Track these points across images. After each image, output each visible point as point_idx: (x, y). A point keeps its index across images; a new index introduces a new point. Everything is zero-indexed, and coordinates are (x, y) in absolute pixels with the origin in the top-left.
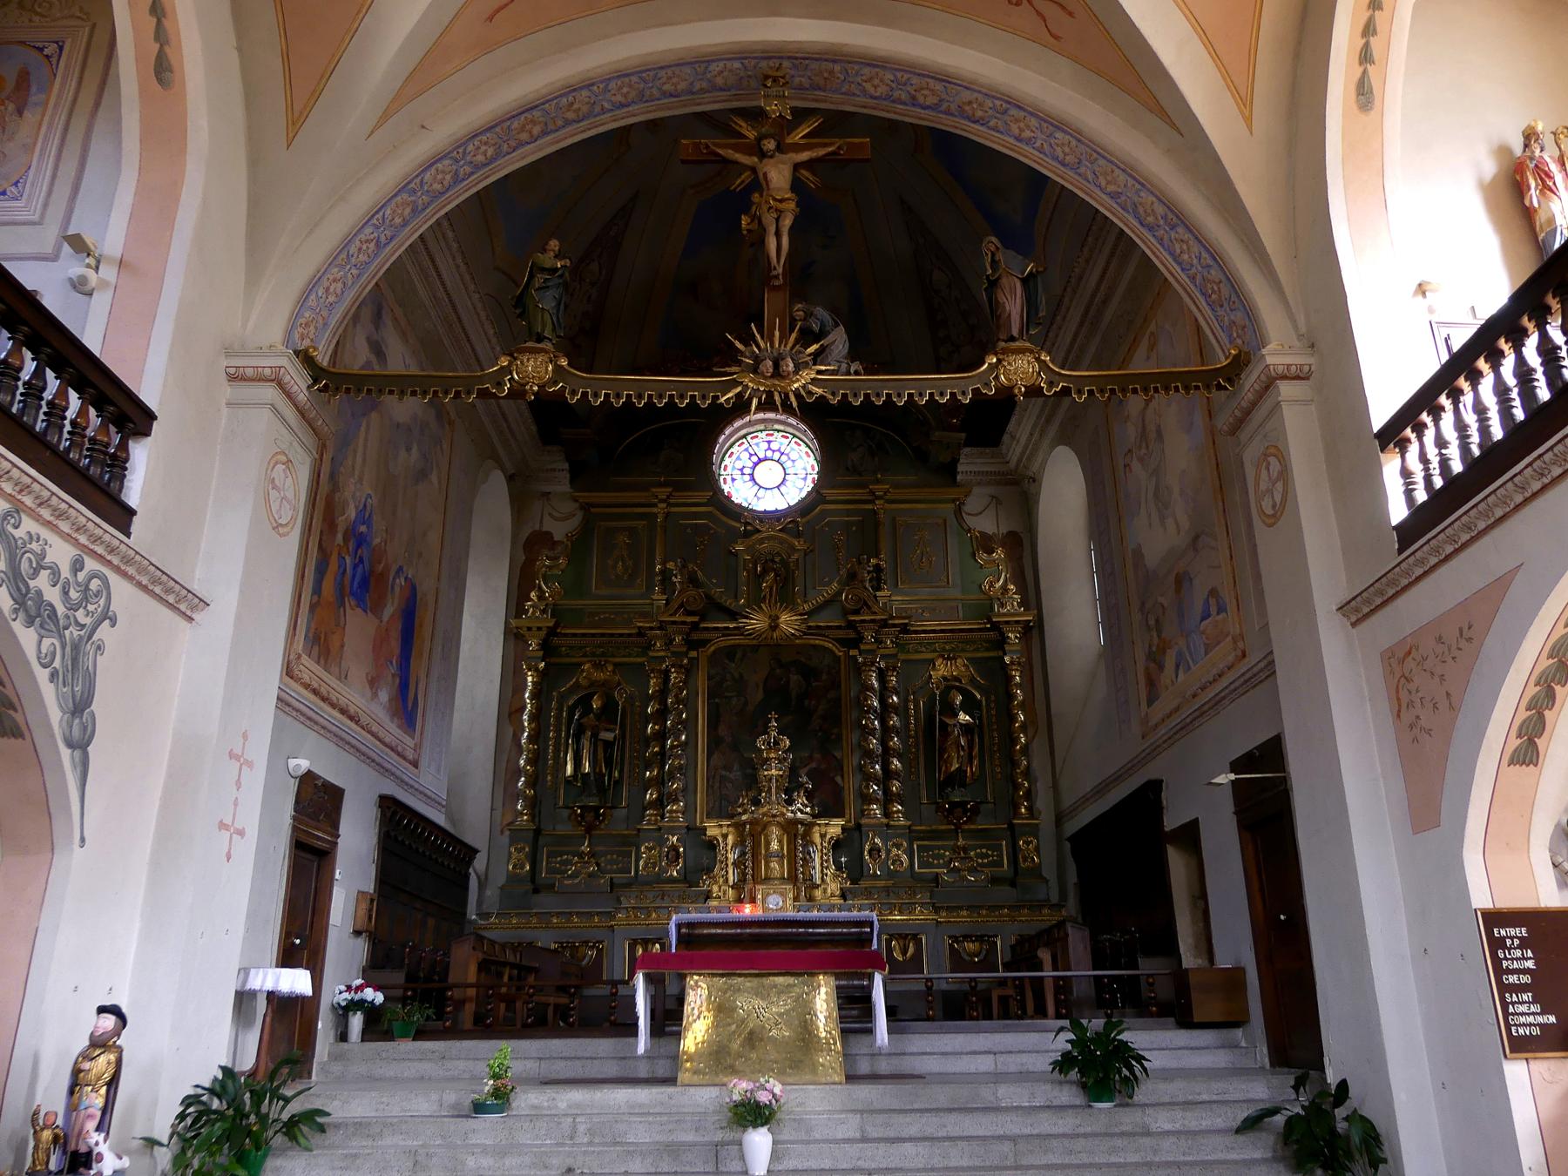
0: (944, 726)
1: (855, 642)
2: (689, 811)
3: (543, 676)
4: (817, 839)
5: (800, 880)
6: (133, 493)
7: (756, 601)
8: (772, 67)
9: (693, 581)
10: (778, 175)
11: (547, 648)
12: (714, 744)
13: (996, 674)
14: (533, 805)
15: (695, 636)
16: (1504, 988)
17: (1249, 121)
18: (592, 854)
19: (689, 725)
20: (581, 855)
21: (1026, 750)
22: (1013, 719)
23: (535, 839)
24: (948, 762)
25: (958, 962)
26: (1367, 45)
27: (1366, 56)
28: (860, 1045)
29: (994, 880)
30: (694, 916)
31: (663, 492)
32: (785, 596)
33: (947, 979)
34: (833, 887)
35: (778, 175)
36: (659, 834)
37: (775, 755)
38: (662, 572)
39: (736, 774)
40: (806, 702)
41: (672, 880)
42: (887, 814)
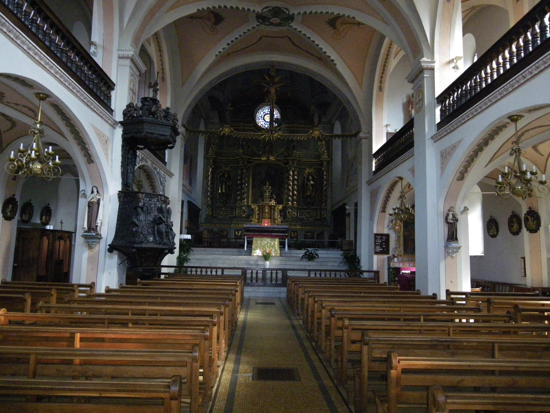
0: (307, 184)
1: (288, 163)
2: (248, 202)
5: (272, 218)
6: (166, 161)
8: (272, 64)
10: (273, 91)
11: (214, 162)
13: (320, 172)
14: (212, 199)
16: (375, 245)
17: (361, 88)
20: (223, 211)
22: (323, 183)
25: (306, 237)
26: (381, 80)
27: (381, 82)
28: (283, 251)
29: (316, 220)
30: (248, 226)
31: (242, 124)
33: (301, 239)
34: (279, 220)
35: (273, 91)
36: (241, 207)
37: (268, 190)
40: (275, 178)
41: (244, 217)
42: (292, 204)
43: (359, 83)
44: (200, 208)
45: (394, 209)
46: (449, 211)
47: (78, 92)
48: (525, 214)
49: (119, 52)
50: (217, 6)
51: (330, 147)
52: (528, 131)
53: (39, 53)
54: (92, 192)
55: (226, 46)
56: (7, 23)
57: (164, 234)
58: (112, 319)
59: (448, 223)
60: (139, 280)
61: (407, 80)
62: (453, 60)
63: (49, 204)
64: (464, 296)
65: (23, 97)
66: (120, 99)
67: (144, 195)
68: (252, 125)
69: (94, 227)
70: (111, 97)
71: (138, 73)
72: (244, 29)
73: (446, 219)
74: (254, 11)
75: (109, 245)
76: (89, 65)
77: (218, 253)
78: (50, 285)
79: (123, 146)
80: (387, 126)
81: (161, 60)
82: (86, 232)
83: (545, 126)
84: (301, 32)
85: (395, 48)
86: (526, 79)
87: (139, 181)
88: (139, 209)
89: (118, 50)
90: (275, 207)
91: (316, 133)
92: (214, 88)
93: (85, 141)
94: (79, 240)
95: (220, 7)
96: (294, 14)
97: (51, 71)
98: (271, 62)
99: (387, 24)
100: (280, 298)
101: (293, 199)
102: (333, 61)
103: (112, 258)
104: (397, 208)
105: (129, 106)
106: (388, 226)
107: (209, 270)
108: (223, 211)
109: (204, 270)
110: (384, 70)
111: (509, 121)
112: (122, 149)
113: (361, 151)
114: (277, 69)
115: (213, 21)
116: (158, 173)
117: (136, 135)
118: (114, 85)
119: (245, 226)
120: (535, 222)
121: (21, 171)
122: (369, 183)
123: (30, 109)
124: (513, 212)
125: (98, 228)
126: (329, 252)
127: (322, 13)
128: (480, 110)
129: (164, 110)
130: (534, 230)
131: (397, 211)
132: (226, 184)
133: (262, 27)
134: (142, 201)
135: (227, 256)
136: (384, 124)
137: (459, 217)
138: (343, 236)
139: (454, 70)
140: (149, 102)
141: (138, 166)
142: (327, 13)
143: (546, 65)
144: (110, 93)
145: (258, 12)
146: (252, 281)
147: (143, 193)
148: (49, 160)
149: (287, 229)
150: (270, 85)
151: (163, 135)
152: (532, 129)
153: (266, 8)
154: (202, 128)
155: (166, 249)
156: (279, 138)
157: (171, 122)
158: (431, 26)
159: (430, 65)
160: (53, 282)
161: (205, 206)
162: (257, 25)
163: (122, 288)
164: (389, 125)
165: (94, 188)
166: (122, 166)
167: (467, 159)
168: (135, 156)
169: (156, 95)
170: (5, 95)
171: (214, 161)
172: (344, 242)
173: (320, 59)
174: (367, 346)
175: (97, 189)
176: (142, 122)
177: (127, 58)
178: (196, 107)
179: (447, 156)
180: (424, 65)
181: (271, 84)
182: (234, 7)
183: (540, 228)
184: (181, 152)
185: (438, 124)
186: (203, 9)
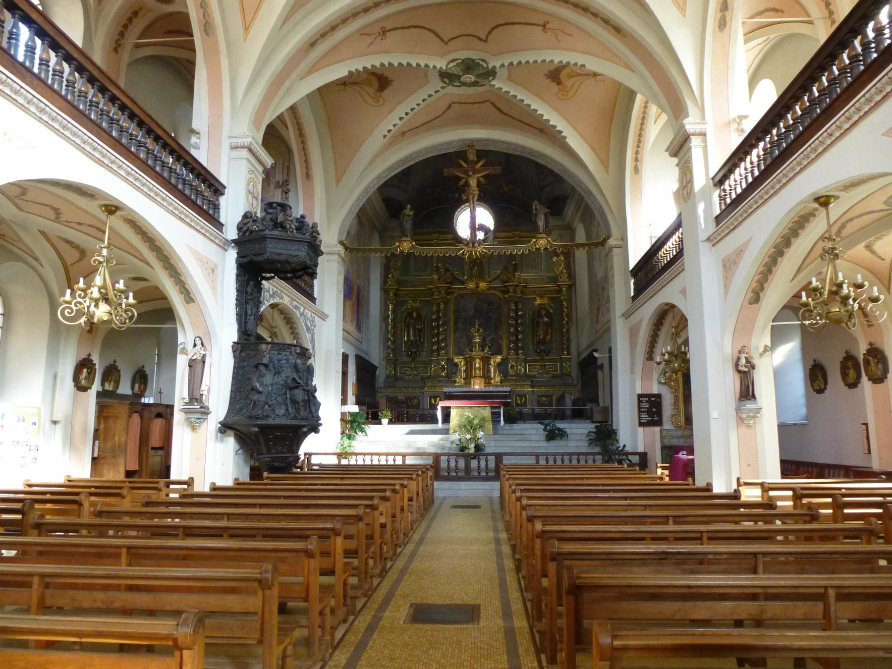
0: (538, 322)
3: (395, 305)
4: (492, 363)
5: (487, 378)
6: (315, 296)
7: (471, 277)
8: (471, 144)
9: (447, 270)
10: (473, 183)
12: (456, 329)
15: (449, 290)
16: (640, 412)
17: (607, 172)
18: (415, 368)
23: (393, 362)
25: (540, 404)
27: (636, 160)
29: (554, 377)
30: (451, 390)
31: (436, 236)
32: (481, 276)
34: (498, 379)
35: (473, 183)
38: (437, 266)
39: (464, 340)
41: (443, 377)
43: (602, 161)
46: (740, 352)
47: (164, 199)
50: (378, 65)
51: (572, 265)
52: (851, 220)
54: (195, 345)
56: (47, 108)
57: (301, 404)
58: (189, 528)
59: (739, 372)
60: (265, 474)
61: (667, 153)
63: (143, 367)
65: (85, 211)
67: (269, 346)
70: (219, 205)
71: (261, 169)
73: (737, 365)
74: (434, 67)
75: (220, 423)
79: (238, 276)
82: (187, 404)
86: (833, 138)
88: (262, 368)
89: (230, 138)
91: (542, 242)
94: (178, 417)
96: (494, 67)
98: (469, 140)
99: (633, 71)
102: (561, 132)
105: (246, 216)
108: (411, 368)
110: (639, 141)
111: (816, 205)
113: (612, 267)
114: (478, 151)
115: (377, 87)
116: (302, 314)
117: (255, 259)
118: (225, 187)
119: (445, 390)
120: (880, 366)
124: (847, 352)
125: (204, 397)
127: (536, 62)
128: (772, 192)
129: (297, 219)
130: (878, 379)
131: (666, 357)
132: (414, 329)
133: (450, 89)
134: (268, 356)
137: (756, 361)
138: (595, 400)
140: (275, 208)
141: (267, 304)
142: (544, 61)
143: (861, 114)
144: (218, 200)
145: (441, 68)
152: (858, 217)
153: (452, 61)
155: (304, 426)
157: (307, 236)
161: (384, 363)
162: (442, 88)
163: (238, 484)
167: (761, 269)
168: (259, 288)
170: (61, 211)
171: (395, 295)
173: (542, 131)
174: (555, 563)
175: (201, 339)
176: (264, 238)
183: (889, 375)
184: (338, 281)
185: (717, 218)
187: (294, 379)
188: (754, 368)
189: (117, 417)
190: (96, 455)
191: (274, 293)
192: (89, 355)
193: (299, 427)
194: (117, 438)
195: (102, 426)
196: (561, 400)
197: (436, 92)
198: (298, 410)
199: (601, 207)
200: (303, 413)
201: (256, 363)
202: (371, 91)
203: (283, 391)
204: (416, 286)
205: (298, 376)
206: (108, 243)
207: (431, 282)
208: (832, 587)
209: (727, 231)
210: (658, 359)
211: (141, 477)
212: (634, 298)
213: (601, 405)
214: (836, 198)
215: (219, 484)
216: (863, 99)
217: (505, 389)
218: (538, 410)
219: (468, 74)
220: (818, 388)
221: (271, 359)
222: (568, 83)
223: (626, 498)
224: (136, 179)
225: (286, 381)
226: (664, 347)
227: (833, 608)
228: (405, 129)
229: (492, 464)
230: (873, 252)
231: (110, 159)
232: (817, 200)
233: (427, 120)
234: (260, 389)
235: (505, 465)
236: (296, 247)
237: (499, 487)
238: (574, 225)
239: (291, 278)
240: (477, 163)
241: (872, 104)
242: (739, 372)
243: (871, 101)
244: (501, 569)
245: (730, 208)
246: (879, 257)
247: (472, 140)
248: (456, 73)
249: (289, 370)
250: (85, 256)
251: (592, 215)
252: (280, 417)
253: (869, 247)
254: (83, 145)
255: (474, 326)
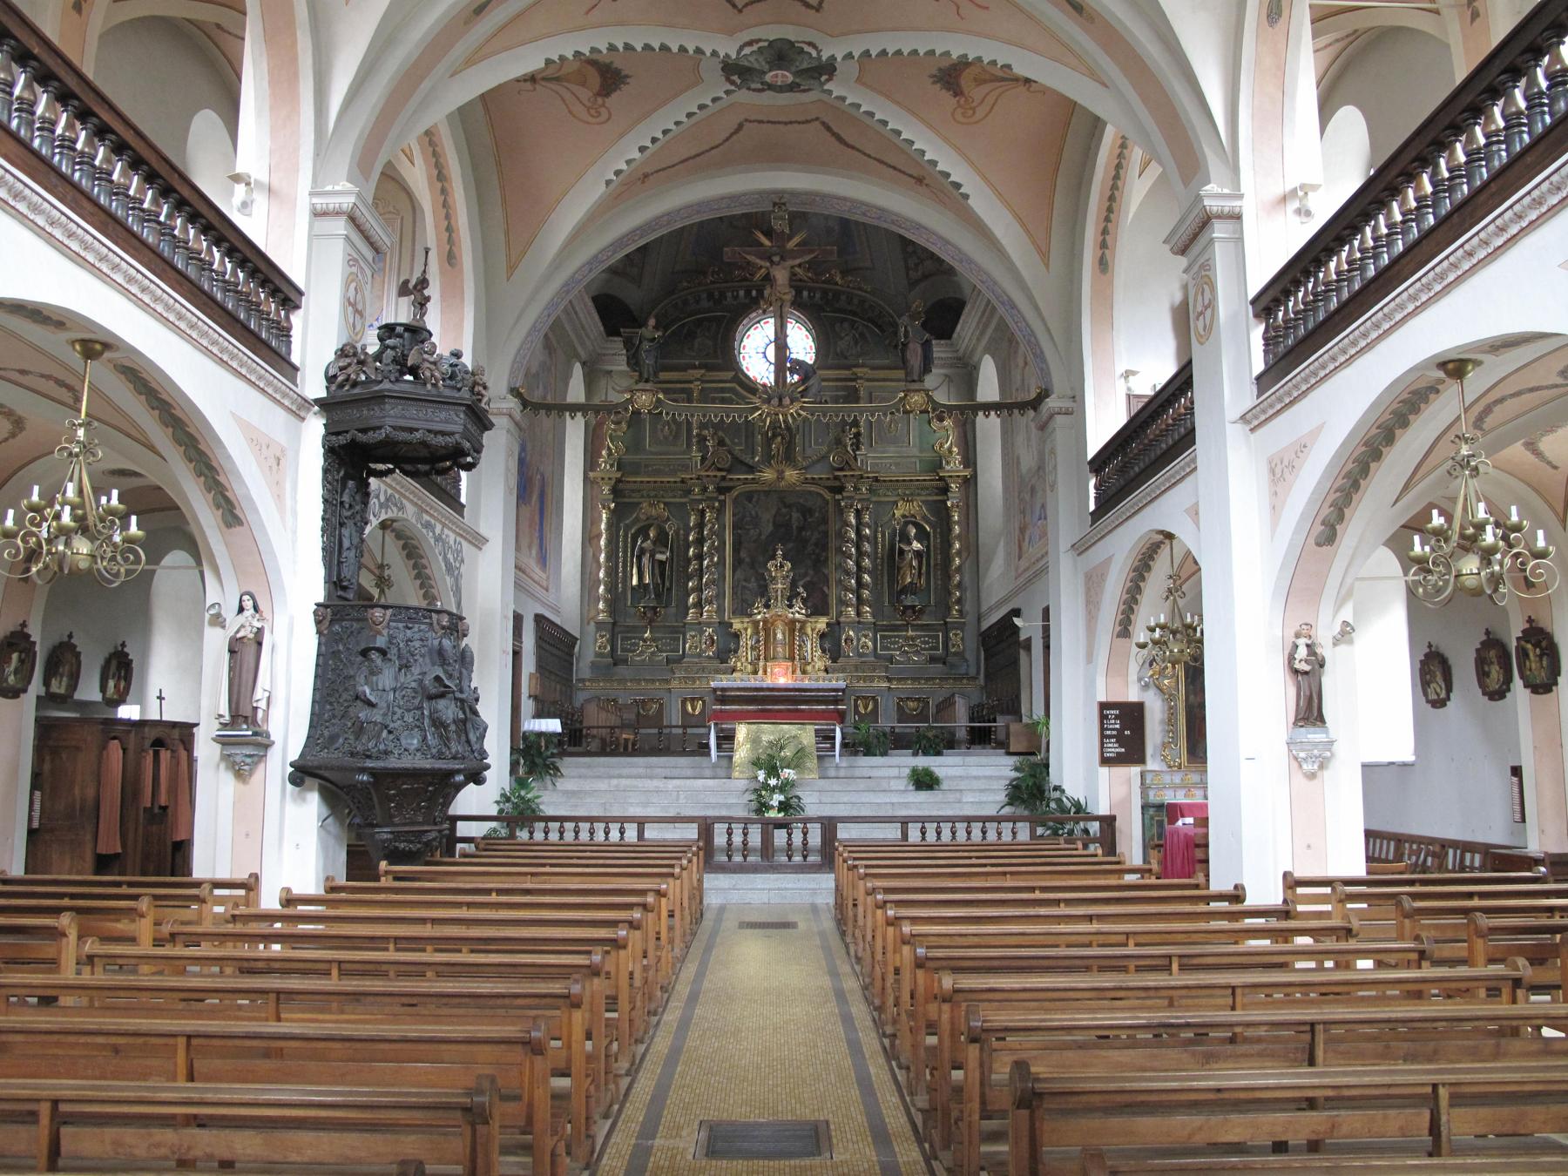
0: (902, 552)
1: (840, 490)
2: (720, 610)
4: (809, 631)
6: (463, 500)
7: (768, 458)
8: (779, 200)
9: (721, 443)
10: (781, 275)
11: (616, 492)
13: (941, 513)
14: (614, 605)
15: (724, 484)
16: (1103, 737)
17: (1047, 265)
19: (720, 550)
21: (959, 569)
22: (950, 546)
23: (614, 628)
24: (904, 579)
25: (903, 716)
27: (1104, 245)
31: (698, 373)
34: (820, 664)
35: (781, 275)
37: (779, 571)
39: (753, 585)
41: (709, 657)
42: (859, 614)
44: (577, 635)
45: (1152, 630)
46: (1298, 636)
47: (192, 327)
48: (1518, 639)
49: (315, 200)
50: (603, 48)
52: (1501, 400)
53: (80, 231)
54: (241, 610)
55: (636, 155)
60: (383, 865)
62: (1294, 192)
64: (1328, 890)
66: (316, 339)
67: (389, 612)
68: (730, 374)
69: (249, 713)
72: (689, 103)
73: (1291, 658)
74: (715, 53)
76: (226, 245)
77: (634, 771)
78: (131, 884)
79: (326, 471)
80: (1128, 374)
81: (445, 204)
82: (224, 726)
83: (1547, 387)
84: (859, 106)
85: (1137, 154)
86: (1475, 261)
87: (381, 567)
88: (374, 655)
90: (803, 623)
92: (613, 271)
93: (214, 464)
94: (205, 750)
95: (612, 48)
96: (833, 58)
97: (114, 277)
100: (814, 909)
101: (859, 597)
102: (957, 186)
103: (304, 800)
104: (1158, 625)
106: (1140, 680)
107: (600, 827)
109: (584, 826)
110: (1110, 210)
111: (1441, 374)
112: (325, 479)
116: (438, 539)
117: (361, 437)
118: (301, 293)
121: (37, 562)
122: (1081, 548)
123: (61, 383)
125: (260, 714)
126: (971, 760)
128: (1363, 344)
133: (743, 96)
134: (385, 632)
135: (656, 783)
136: (1116, 379)
137: (1326, 650)
138: (1014, 709)
139: (1297, 219)
140: (400, 336)
141: (375, 522)
142: (932, 52)
143: (1524, 224)
145: (727, 55)
146: (730, 857)
147: (385, 607)
148: (111, 528)
149: (843, 690)
150: (772, 262)
151: (443, 433)
153: (750, 43)
154: (576, 391)
155: (458, 771)
156: (805, 420)
157: (465, 393)
158: (1226, 99)
159: (1227, 205)
160: (144, 874)
162: (727, 92)
164: (1134, 373)
165: (246, 597)
166: (324, 530)
167: (1340, 482)
168: (364, 492)
169: (423, 315)
172: (1014, 727)
173: (919, 180)
177: (338, 213)
178: (556, 326)
179: (1287, 475)
180: (1212, 204)
181: (776, 259)
182: (656, 46)
183: (1560, 679)
184: (507, 469)
185: (1258, 378)
186: (562, 58)
187: (437, 679)
188: (1322, 666)
189: (78, 749)
190: (36, 825)
191: (387, 500)
192: (24, 625)
193: (451, 773)
194: (77, 791)
195: (47, 767)
196: (946, 705)
197: (714, 100)
198: (446, 741)
199: (1033, 334)
200: (455, 747)
201: (363, 646)
202: (585, 94)
203: (416, 702)
204: (658, 472)
205: (446, 672)
206: (87, 415)
207: (686, 468)
208: (1444, 1085)
209: (1279, 407)
210: (1142, 636)
211: (124, 874)
212: (1096, 515)
213: (1025, 720)
214: (1477, 363)
215: (299, 890)
216: (1527, 200)
217: (834, 684)
218: (900, 727)
219: (780, 68)
220: (1433, 697)
221: (391, 637)
222: (977, 93)
223: (1090, 918)
224: (144, 290)
225: (421, 681)
226: (1152, 612)
227: (1444, 1118)
228: (648, 170)
229: (815, 838)
230: (1538, 453)
231: (98, 253)
232: (1442, 365)
233: (693, 153)
234: (372, 699)
235: (840, 841)
236: (443, 415)
237: (832, 885)
238: (976, 359)
239: (427, 474)
240: (790, 238)
241: (1544, 209)
242: (1296, 672)
243: (1540, 204)
244: (855, 1047)
245: (1283, 362)
246: (1549, 463)
247: (780, 193)
248: (756, 66)
249: (427, 660)
250: (22, 429)
251: (1012, 341)
252: (411, 751)
253: (1531, 446)
254: (49, 229)
255: (773, 557)
